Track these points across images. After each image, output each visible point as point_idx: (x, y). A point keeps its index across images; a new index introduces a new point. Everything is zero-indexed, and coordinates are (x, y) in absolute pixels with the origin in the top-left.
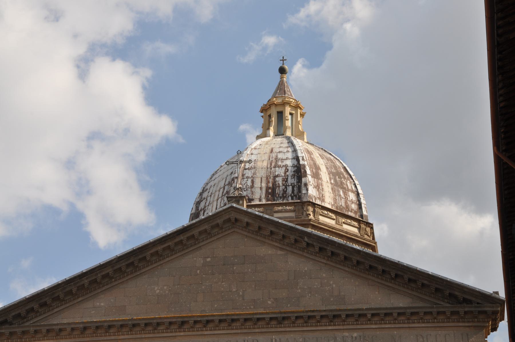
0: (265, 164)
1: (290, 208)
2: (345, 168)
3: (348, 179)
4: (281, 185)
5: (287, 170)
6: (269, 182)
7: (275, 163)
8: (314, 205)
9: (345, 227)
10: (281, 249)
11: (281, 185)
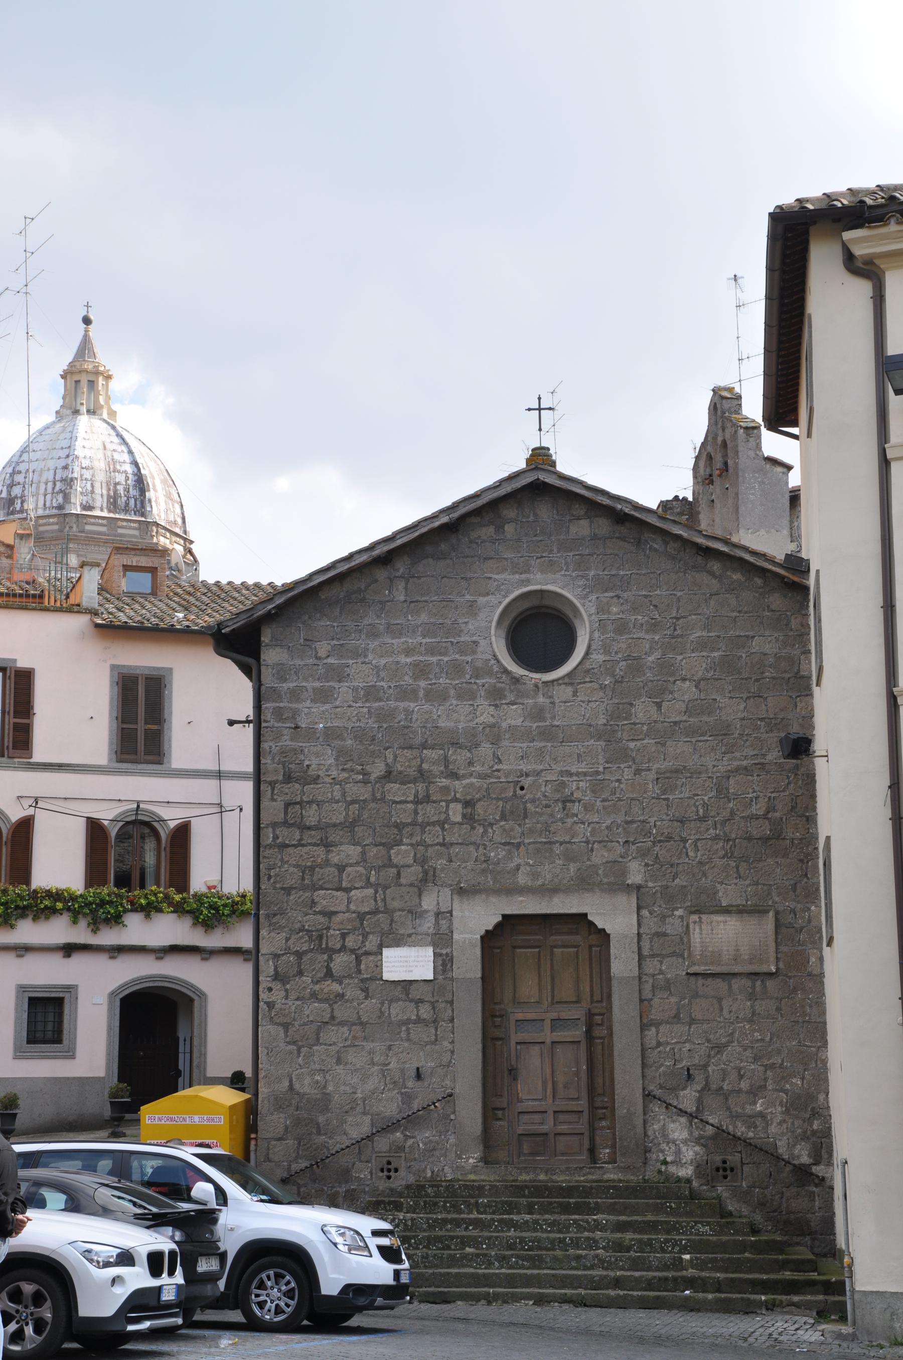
5: (127, 479)
7: (112, 466)
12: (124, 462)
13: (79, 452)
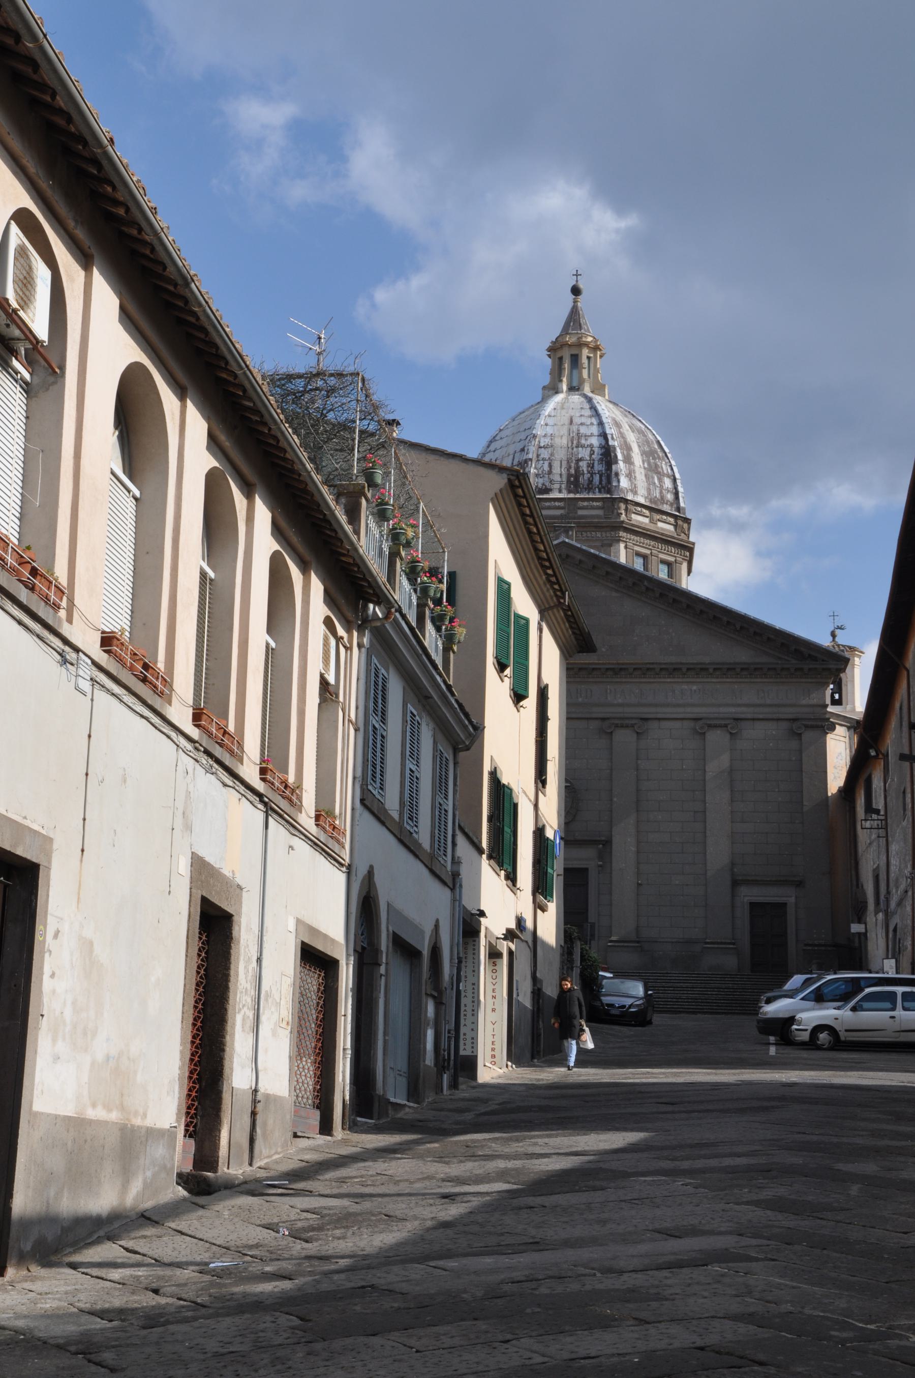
0: (564, 441)
1: (598, 504)
2: (658, 442)
3: (663, 459)
4: (585, 472)
5: (592, 453)
6: (570, 467)
7: (577, 440)
8: (626, 501)
9: (660, 524)
10: (617, 591)
11: (585, 472)
12: (592, 435)
13: (539, 431)
